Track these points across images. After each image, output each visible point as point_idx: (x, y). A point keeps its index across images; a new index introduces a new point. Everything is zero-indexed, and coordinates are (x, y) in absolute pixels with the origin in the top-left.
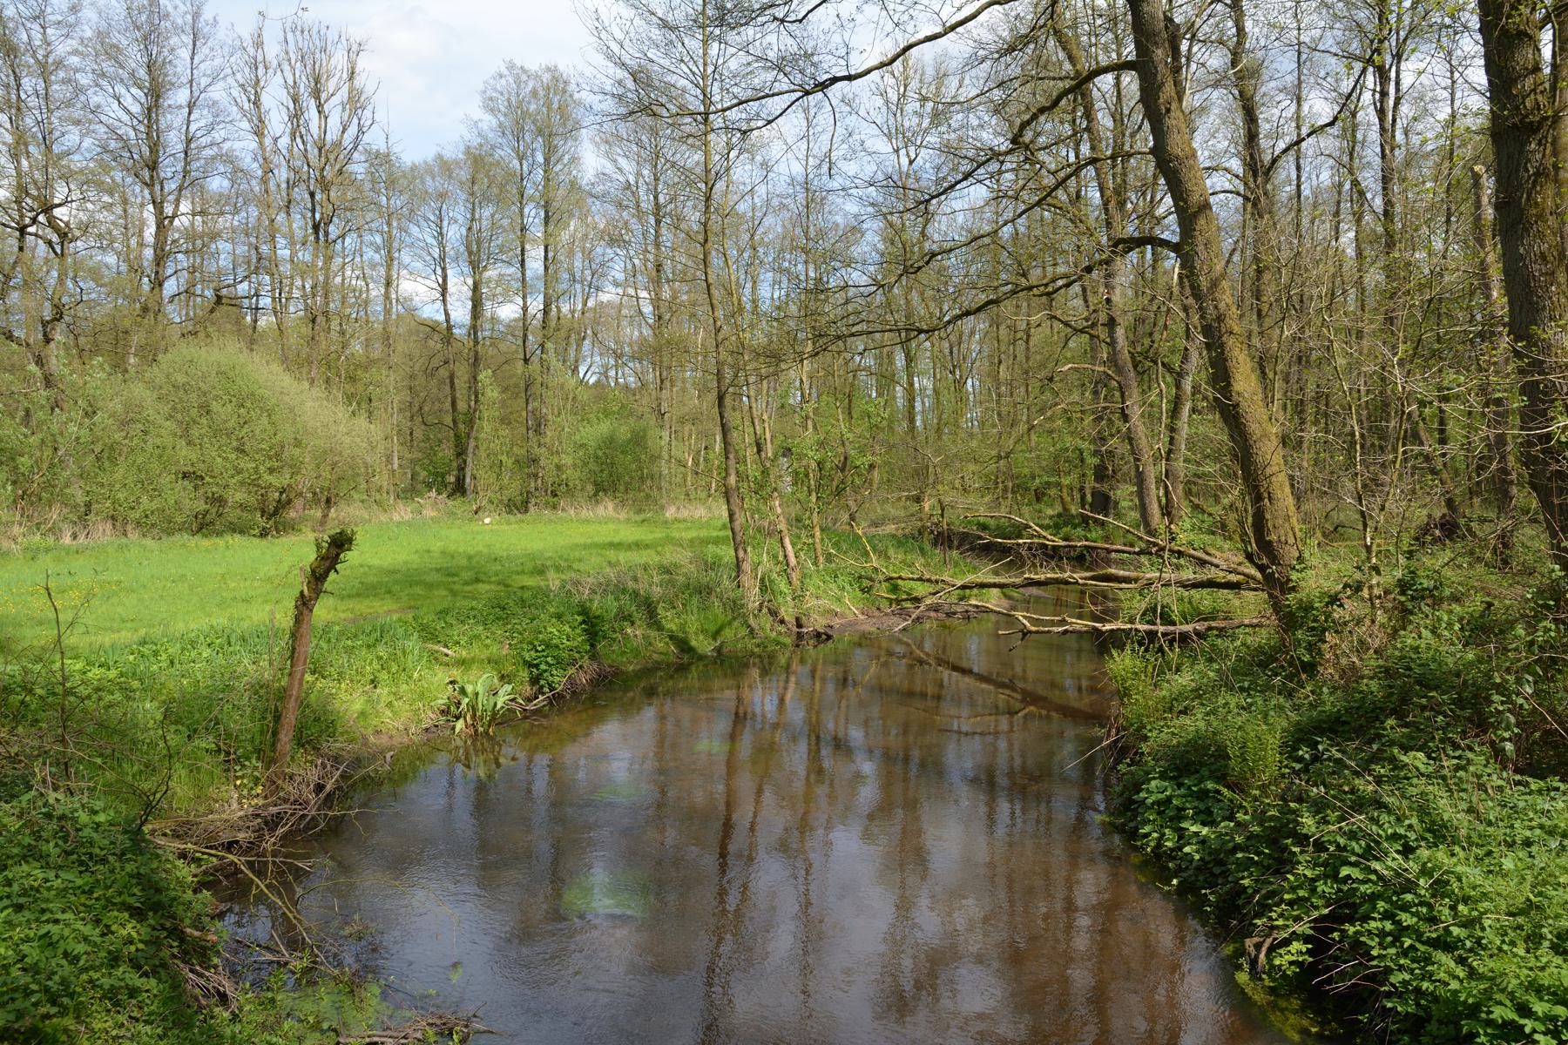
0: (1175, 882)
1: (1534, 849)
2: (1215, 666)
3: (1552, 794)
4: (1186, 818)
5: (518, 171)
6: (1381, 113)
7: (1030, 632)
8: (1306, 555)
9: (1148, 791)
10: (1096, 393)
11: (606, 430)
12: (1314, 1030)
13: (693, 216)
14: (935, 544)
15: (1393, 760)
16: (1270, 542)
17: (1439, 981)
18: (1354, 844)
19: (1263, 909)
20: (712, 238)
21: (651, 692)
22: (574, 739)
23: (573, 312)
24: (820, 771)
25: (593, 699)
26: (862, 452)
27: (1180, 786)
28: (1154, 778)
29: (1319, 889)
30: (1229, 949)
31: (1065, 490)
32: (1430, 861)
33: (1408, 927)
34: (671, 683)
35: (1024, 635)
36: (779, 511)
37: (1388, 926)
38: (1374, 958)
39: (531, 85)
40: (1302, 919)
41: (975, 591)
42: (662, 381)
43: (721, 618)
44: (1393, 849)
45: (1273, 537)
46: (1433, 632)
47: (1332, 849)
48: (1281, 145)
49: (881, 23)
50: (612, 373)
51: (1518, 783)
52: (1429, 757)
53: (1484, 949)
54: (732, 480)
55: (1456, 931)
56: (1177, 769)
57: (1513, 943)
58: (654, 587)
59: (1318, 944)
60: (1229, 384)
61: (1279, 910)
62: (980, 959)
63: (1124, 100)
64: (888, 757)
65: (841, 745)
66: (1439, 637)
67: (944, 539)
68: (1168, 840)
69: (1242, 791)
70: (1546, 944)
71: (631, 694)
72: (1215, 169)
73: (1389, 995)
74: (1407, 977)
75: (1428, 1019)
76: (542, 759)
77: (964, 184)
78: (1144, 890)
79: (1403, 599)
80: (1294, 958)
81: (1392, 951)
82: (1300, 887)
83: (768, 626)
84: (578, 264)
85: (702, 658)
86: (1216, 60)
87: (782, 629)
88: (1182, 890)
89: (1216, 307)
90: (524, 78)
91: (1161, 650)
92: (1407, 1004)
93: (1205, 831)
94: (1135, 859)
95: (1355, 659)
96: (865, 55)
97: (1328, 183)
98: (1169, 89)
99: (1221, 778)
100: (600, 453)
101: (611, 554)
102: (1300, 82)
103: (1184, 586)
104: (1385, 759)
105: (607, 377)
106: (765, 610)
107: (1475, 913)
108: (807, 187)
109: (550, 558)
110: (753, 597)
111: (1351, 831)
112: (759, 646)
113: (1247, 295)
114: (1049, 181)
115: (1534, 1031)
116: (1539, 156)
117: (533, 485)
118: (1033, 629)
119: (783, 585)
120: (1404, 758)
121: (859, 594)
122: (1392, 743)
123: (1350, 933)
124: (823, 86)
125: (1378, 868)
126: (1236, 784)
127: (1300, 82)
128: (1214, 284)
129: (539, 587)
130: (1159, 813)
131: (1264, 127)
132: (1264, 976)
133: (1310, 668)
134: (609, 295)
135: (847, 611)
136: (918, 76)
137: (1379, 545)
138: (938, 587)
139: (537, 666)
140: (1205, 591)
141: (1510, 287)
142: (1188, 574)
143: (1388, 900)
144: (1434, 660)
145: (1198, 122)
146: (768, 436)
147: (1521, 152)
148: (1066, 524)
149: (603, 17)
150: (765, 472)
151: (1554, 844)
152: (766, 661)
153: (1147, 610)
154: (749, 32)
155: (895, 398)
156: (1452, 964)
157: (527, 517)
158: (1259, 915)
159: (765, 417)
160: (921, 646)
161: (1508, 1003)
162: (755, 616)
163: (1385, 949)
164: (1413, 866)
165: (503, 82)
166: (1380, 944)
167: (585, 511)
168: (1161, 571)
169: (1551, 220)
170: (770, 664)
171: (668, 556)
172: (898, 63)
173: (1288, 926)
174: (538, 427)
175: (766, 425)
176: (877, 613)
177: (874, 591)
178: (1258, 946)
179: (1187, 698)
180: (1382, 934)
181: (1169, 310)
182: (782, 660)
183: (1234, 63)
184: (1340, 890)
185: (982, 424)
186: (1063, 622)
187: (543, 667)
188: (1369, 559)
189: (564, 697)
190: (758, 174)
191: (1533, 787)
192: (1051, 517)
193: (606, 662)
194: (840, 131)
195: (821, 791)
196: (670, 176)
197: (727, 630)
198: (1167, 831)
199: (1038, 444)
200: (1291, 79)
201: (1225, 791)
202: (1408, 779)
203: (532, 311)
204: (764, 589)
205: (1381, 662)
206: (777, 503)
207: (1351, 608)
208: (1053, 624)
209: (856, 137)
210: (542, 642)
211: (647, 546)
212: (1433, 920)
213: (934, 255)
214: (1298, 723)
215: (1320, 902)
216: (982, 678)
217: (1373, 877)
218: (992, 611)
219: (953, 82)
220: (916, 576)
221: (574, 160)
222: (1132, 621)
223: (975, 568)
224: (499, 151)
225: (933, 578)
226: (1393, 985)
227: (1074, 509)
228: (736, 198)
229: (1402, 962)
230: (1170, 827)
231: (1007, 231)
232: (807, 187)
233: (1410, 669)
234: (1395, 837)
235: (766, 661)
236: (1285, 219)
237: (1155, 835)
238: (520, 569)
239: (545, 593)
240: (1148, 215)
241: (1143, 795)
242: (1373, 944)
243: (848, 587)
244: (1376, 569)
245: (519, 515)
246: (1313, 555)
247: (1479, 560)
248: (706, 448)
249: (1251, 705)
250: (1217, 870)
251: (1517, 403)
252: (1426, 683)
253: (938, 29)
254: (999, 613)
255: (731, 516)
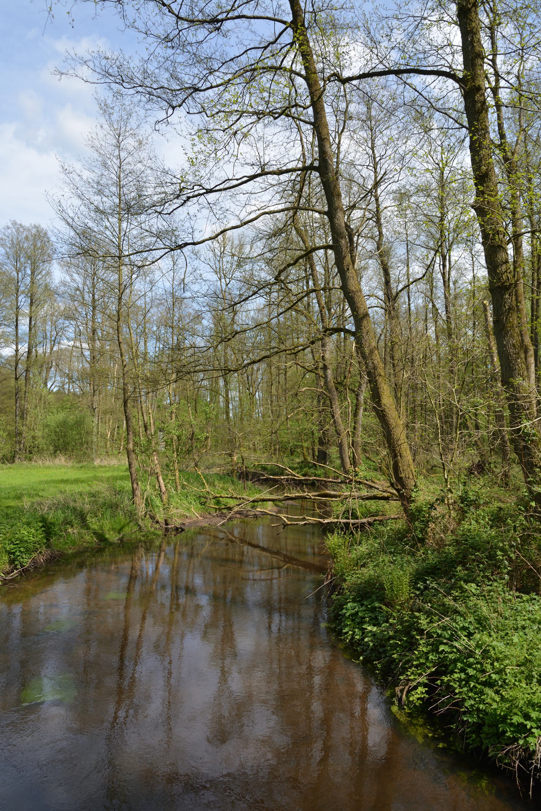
0: (361, 658)
1: (527, 630)
2: (378, 541)
3: (533, 602)
4: (365, 623)
5: (16, 278)
6: (443, 275)
7: (288, 525)
8: (418, 484)
9: (347, 609)
10: (319, 402)
11: (61, 417)
12: (430, 735)
13: (113, 307)
14: (239, 478)
15: (461, 588)
16: (401, 478)
17: (487, 703)
18: (445, 633)
19: (404, 670)
20: (122, 319)
21: (81, 566)
22: (34, 594)
23: (45, 353)
24: (178, 605)
25: (47, 571)
26: (202, 430)
27: (362, 605)
28: (349, 602)
29: (430, 658)
30: (388, 693)
31: (305, 449)
32: (480, 640)
33: (472, 676)
34: (93, 559)
35: (285, 526)
36: (156, 462)
37: (463, 676)
38: (456, 694)
39: (25, 233)
40: (422, 675)
41: (260, 503)
42: (94, 391)
43: (123, 522)
44: (462, 634)
45: (403, 475)
46: (476, 521)
47: (435, 636)
48: (401, 287)
49: (210, 218)
50: (66, 386)
51: (518, 597)
52: (478, 586)
53: (507, 685)
54: (131, 446)
55: (494, 676)
56: (360, 596)
57: (520, 681)
58: (85, 505)
59: (431, 688)
60: (380, 400)
61: (411, 671)
62: (265, 702)
63: (329, 261)
64: (215, 598)
65: (190, 591)
66: (479, 523)
67: (244, 476)
68: (357, 635)
69: (392, 606)
70: (535, 680)
71: (69, 567)
72: (372, 296)
73: (464, 713)
74: (473, 702)
75: (484, 724)
76: (17, 609)
77: (254, 297)
78: (348, 661)
79: (462, 505)
80: (419, 696)
81: (465, 689)
82: (421, 657)
83: (150, 525)
84: (48, 328)
85: (111, 544)
86: (370, 246)
87: (157, 526)
88: (364, 662)
89: (373, 363)
90: (21, 230)
91: (352, 533)
92: (473, 717)
93: (375, 629)
94: (341, 646)
95: (442, 535)
96: (202, 233)
97: (421, 305)
98: (348, 259)
99: (382, 600)
100: (58, 430)
101: (62, 486)
102: (408, 258)
103: (363, 499)
104: (458, 587)
105: (64, 389)
106: (148, 516)
107: (502, 666)
108: (173, 295)
109: (26, 489)
110: (141, 509)
111: (443, 626)
112: (144, 536)
113: (388, 358)
114: (294, 299)
115: (532, 727)
116: (510, 301)
117: (18, 447)
118: (289, 523)
119: (158, 502)
120: (466, 587)
121: (199, 506)
122: (461, 579)
123: (445, 681)
124: (180, 247)
125: (457, 645)
126: (389, 603)
127: (408, 258)
128: (371, 352)
129: (18, 507)
130: (353, 620)
131: (393, 277)
132: (405, 707)
133: (422, 541)
134: (66, 344)
135: (193, 515)
136: (230, 243)
137: (451, 479)
138: (240, 502)
139: (13, 553)
140: (372, 501)
141: (501, 359)
142: (365, 493)
143: (462, 662)
144: (477, 535)
145: (363, 273)
146: (152, 421)
147: (502, 298)
148: (305, 467)
149: (63, 205)
150: (149, 441)
151: (535, 627)
152: (148, 544)
153: (345, 511)
154: (143, 217)
155: (219, 402)
156: (493, 694)
157: (14, 465)
158: (402, 674)
159: (150, 411)
160: (232, 533)
161: (520, 714)
162: (142, 520)
163: (462, 688)
164: (473, 643)
165: (9, 231)
166: (459, 686)
167: (48, 462)
168: (351, 491)
169: (517, 330)
170: (151, 546)
171: (95, 487)
172: (220, 237)
173: (416, 679)
174: (23, 415)
175: (151, 416)
176: (209, 516)
177: (207, 504)
178: (402, 691)
179: (365, 558)
180: (460, 680)
181: (351, 363)
182: (157, 543)
183: (378, 248)
184: (440, 658)
185: (263, 416)
186: (304, 519)
187: (18, 553)
188: (447, 486)
189: (29, 570)
190: (148, 287)
191: (524, 599)
192: (298, 463)
193: (56, 549)
194: (189, 269)
195: (178, 616)
196: (100, 285)
197: (127, 528)
198: (356, 630)
199: (291, 426)
200: (404, 257)
201: (384, 607)
202: (468, 597)
203: (21, 351)
204: (147, 504)
205: (454, 537)
206: (155, 458)
207: (440, 510)
208: (298, 520)
209: (198, 272)
210: (17, 539)
211: (83, 482)
212: (483, 671)
213: (237, 333)
214: (417, 570)
215: (431, 665)
216: (263, 549)
217: (455, 650)
218: (268, 514)
219: (247, 249)
220: (229, 496)
221: (48, 273)
222: (338, 518)
223: (260, 491)
224: (5, 267)
225: (238, 497)
226: (466, 708)
227: (310, 459)
228: (136, 298)
229: (470, 695)
230: (358, 628)
231: (274, 321)
232: (173, 295)
233: (466, 540)
234: (464, 628)
235: (148, 544)
236: (403, 322)
237: (350, 633)
238: (7, 496)
239: (21, 510)
240: (341, 316)
241: (344, 611)
242: (456, 686)
243: (193, 502)
244: (450, 490)
245: (9, 465)
246: (421, 482)
247: (496, 483)
248: (118, 427)
249: (395, 561)
250: (381, 650)
251: (507, 413)
252: (475, 548)
253: (239, 223)
254: (272, 515)
255: (130, 464)
